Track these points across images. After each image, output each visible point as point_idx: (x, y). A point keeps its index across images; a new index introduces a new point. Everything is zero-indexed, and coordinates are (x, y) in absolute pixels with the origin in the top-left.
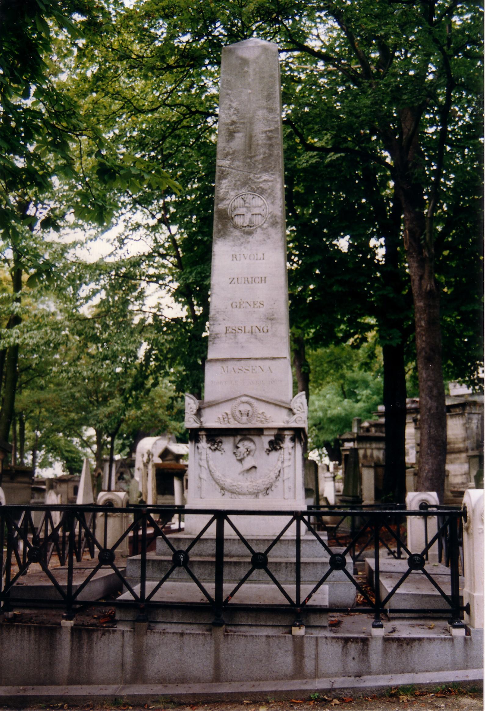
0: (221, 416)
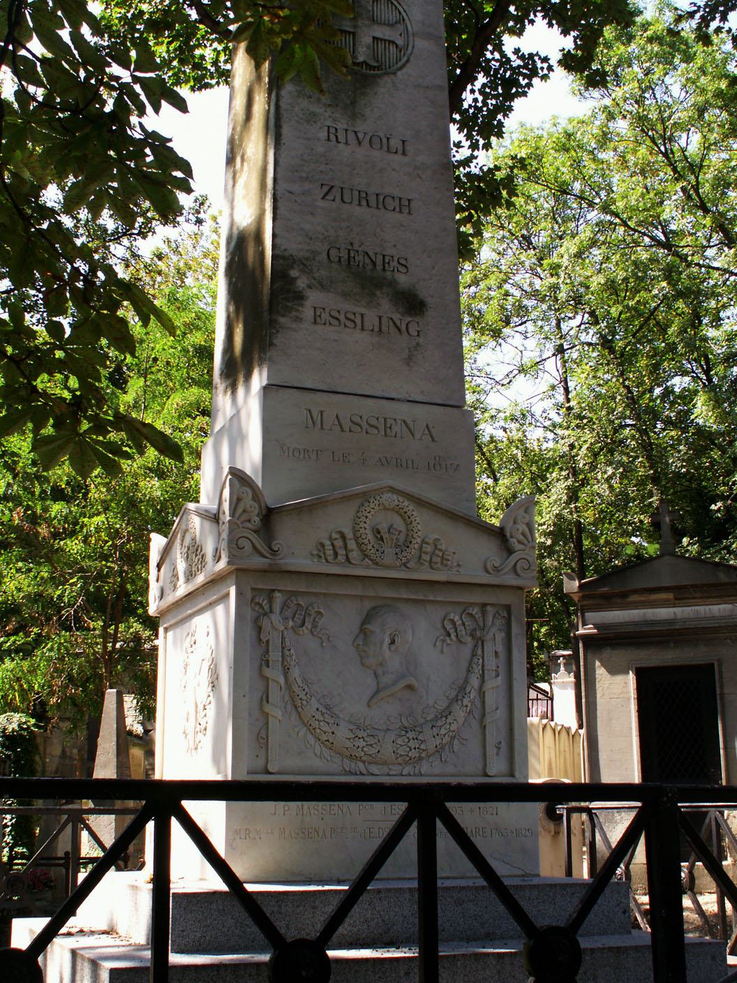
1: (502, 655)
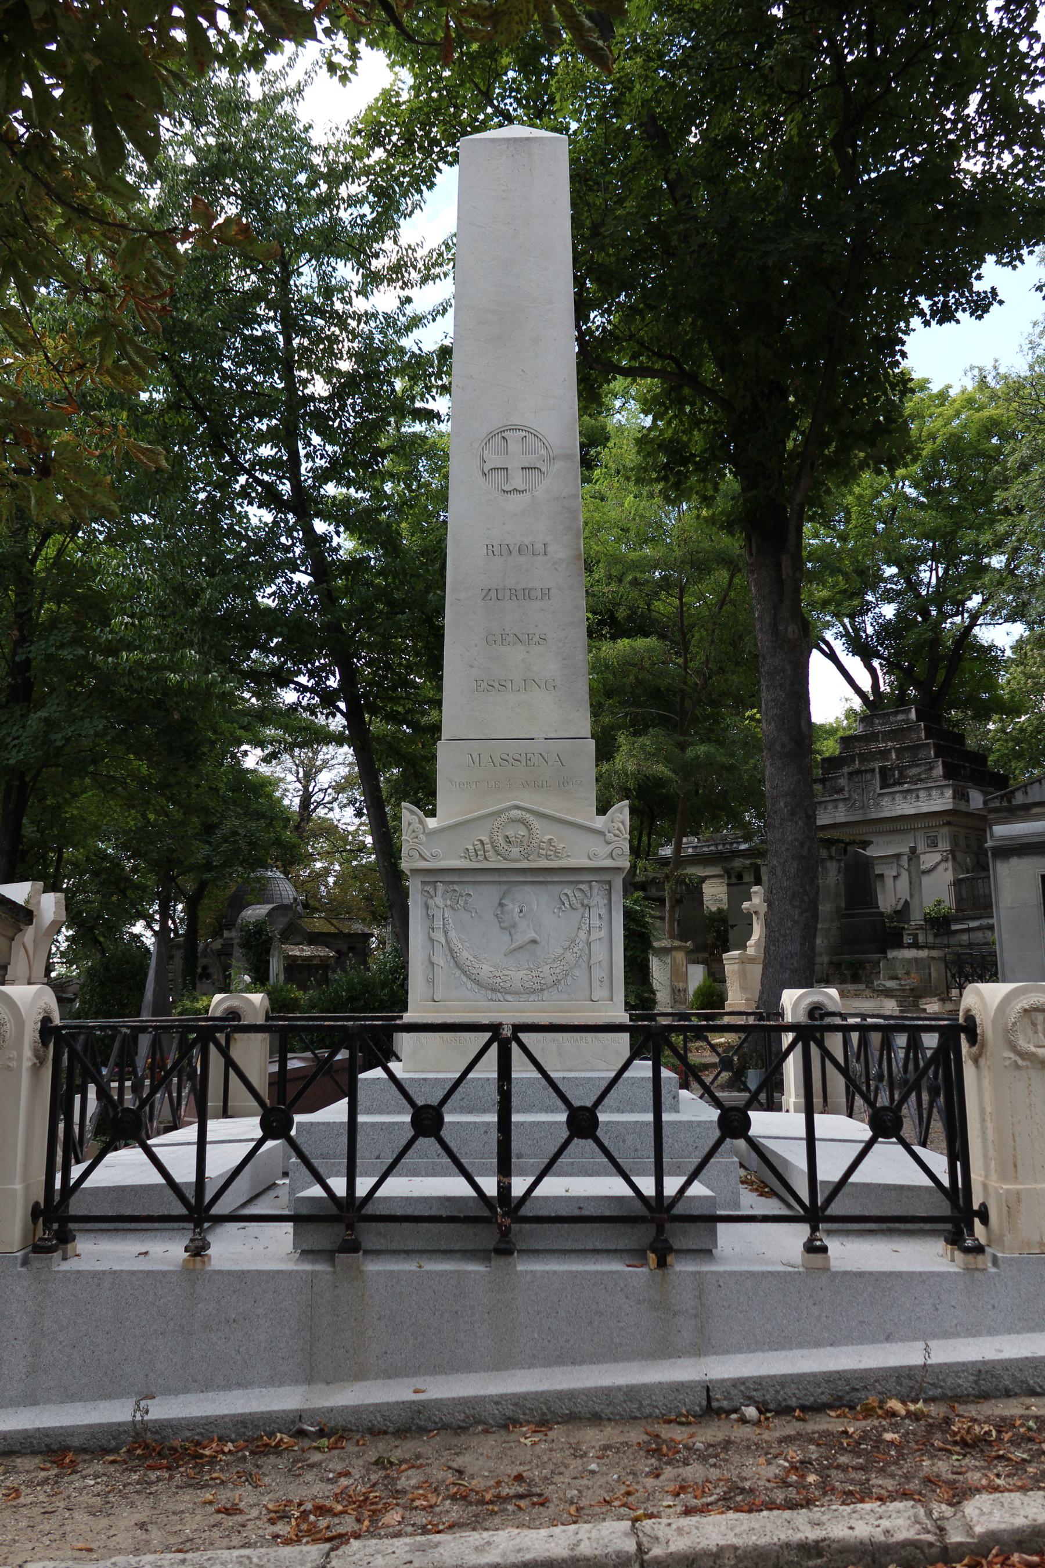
0: (470, 847)
1: (605, 916)
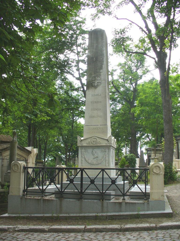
0: (88, 142)
